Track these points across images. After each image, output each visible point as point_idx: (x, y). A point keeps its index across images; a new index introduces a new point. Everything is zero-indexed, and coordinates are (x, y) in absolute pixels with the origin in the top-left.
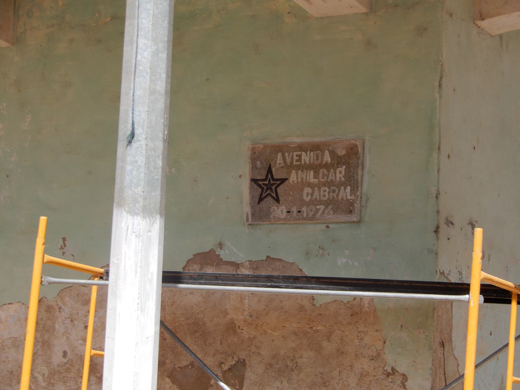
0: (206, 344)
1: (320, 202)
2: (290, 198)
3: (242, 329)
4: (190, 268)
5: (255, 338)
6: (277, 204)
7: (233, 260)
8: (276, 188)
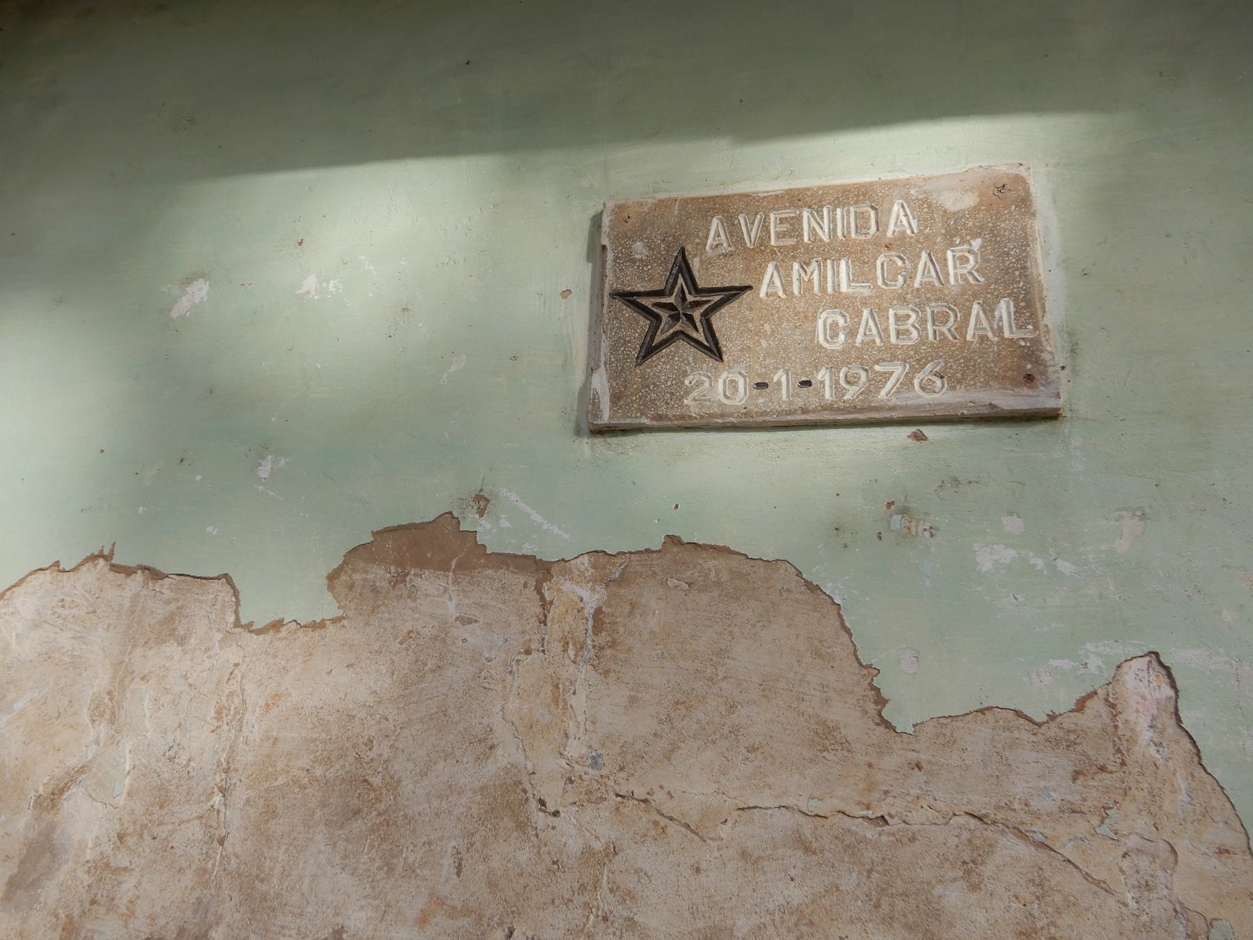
0: (391, 869)
1: (891, 354)
2: (764, 344)
3: (556, 814)
4: (357, 576)
5: (613, 851)
6: (710, 362)
7: (527, 549)
8: (706, 316)
